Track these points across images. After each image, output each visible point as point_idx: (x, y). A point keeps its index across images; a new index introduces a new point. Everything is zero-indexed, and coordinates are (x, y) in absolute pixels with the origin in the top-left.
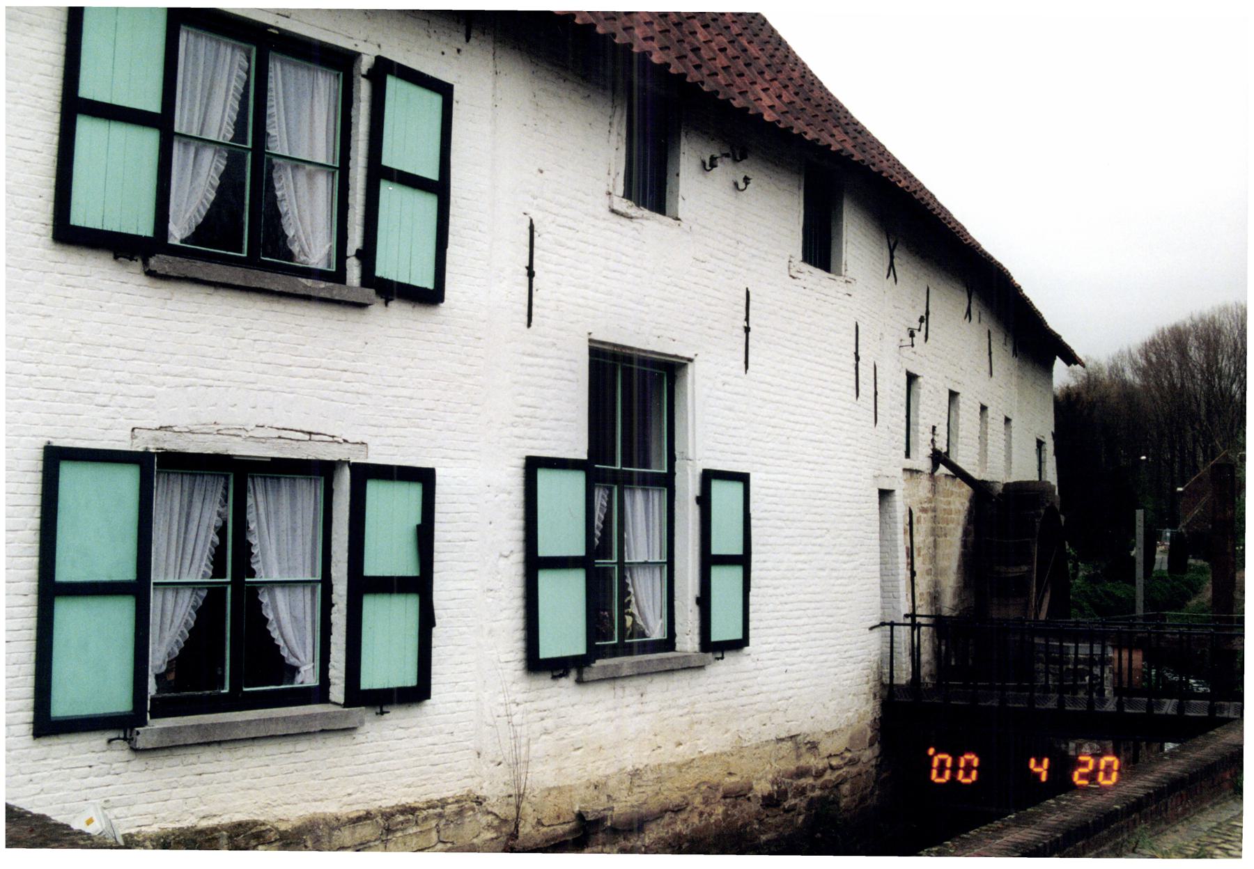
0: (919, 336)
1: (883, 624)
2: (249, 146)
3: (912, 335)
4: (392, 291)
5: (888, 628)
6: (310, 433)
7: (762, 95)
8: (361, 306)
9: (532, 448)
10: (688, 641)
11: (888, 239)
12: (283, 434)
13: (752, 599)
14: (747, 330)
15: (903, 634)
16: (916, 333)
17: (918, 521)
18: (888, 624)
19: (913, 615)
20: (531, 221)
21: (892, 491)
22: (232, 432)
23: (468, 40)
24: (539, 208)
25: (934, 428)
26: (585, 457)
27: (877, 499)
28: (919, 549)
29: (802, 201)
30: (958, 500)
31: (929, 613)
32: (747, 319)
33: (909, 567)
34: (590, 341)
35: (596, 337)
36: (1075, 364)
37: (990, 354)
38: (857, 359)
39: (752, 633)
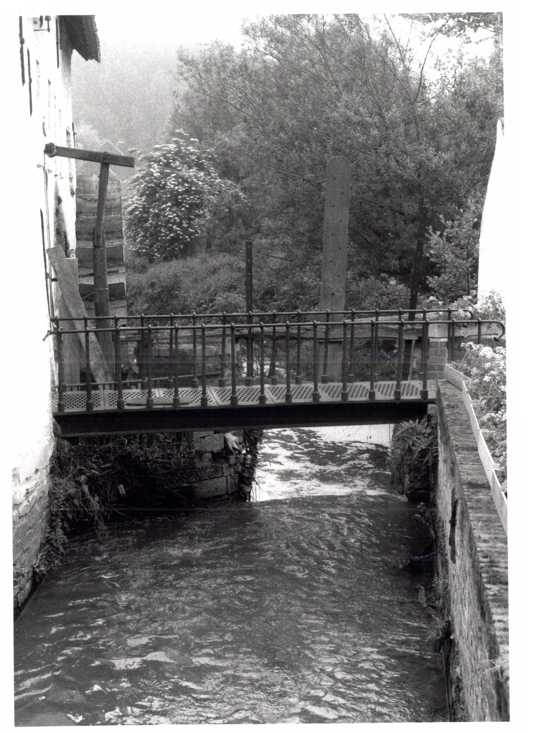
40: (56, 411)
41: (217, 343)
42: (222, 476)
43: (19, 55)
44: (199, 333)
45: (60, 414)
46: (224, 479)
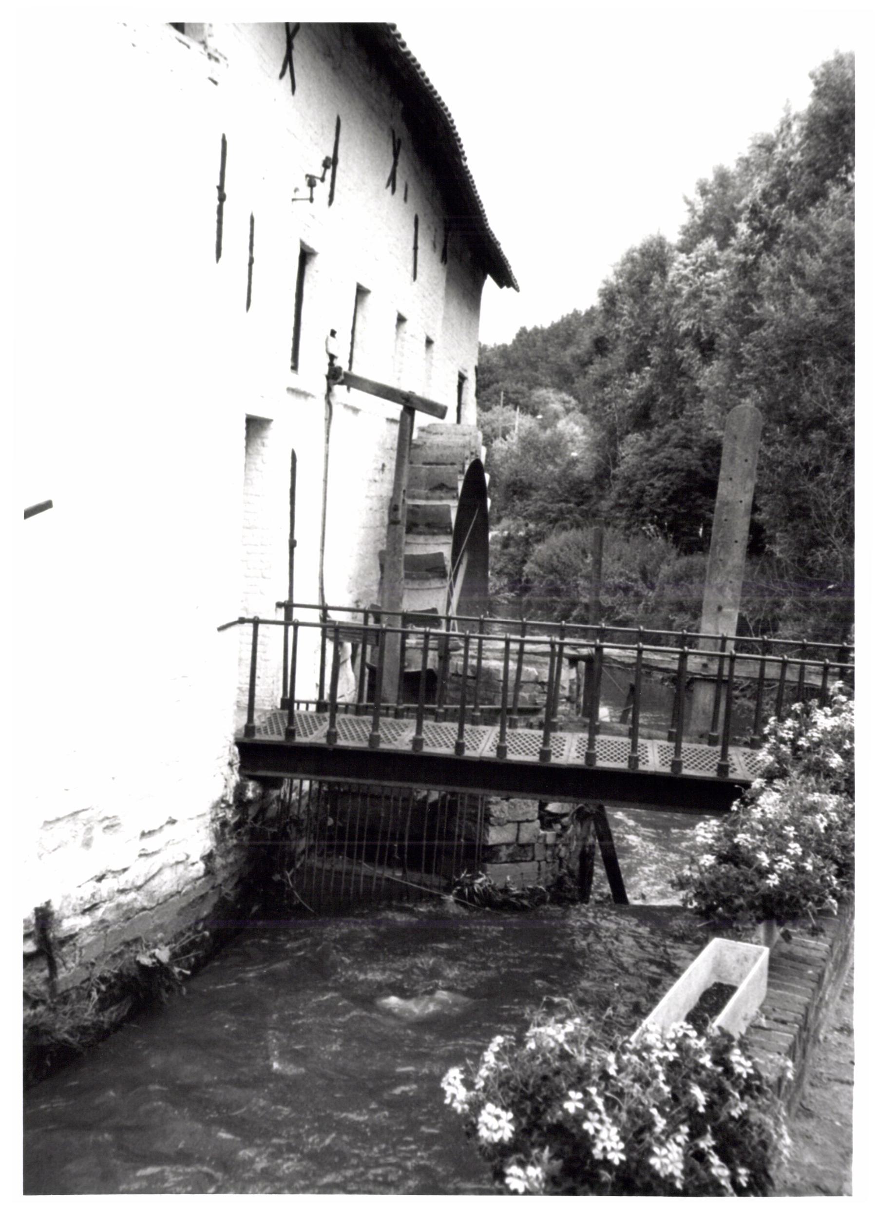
0: (322, 190)
1: (242, 621)
3: (311, 183)
5: (249, 627)
16: (318, 182)
18: (249, 621)
19: (288, 607)
21: (268, 421)
27: (244, 433)
36: (508, 286)
37: (416, 248)
40: (241, 736)
41: (541, 664)
42: (533, 859)
43: (215, 217)
44: (514, 646)
45: (246, 740)
46: (535, 863)
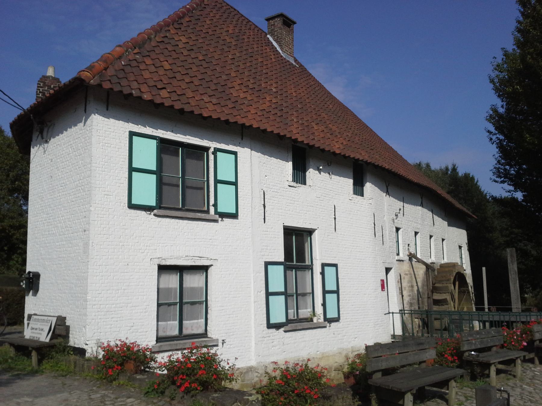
2: (181, 176)
4: (223, 215)
6: (201, 257)
7: (336, 144)
8: (216, 221)
9: (267, 259)
10: (319, 318)
11: (385, 182)
12: (194, 258)
13: (340, 304)
14: (335, 218)
15: (397, 317)
17: (404, 278)
20: (264, 191)
22: (179, 258)
23: (242, 139)
24: (266, 187)
25: (409, 245)
26: (283, 261)
28: (405, 288)
29: (352, 175)
30: (421, 270)
31: (409, 309)
32: (335, 215)
33: (401, 294)
34: (284, 226)
35: (285, 225)
38: (375, 225)
39: (341, 315)
